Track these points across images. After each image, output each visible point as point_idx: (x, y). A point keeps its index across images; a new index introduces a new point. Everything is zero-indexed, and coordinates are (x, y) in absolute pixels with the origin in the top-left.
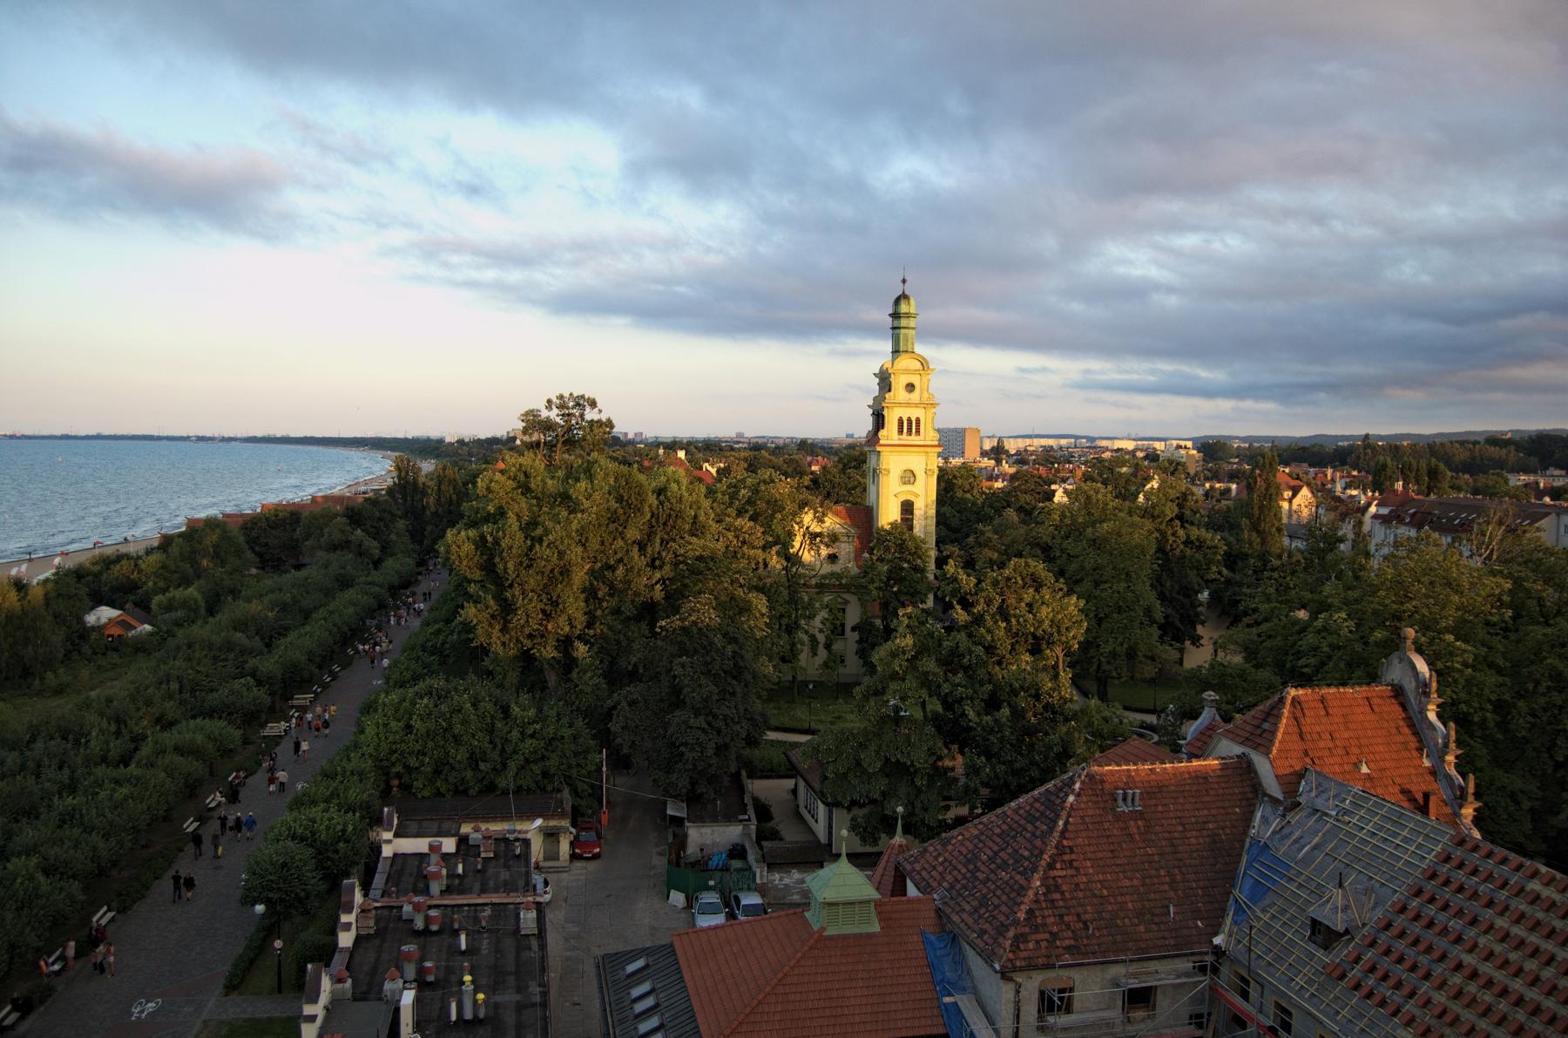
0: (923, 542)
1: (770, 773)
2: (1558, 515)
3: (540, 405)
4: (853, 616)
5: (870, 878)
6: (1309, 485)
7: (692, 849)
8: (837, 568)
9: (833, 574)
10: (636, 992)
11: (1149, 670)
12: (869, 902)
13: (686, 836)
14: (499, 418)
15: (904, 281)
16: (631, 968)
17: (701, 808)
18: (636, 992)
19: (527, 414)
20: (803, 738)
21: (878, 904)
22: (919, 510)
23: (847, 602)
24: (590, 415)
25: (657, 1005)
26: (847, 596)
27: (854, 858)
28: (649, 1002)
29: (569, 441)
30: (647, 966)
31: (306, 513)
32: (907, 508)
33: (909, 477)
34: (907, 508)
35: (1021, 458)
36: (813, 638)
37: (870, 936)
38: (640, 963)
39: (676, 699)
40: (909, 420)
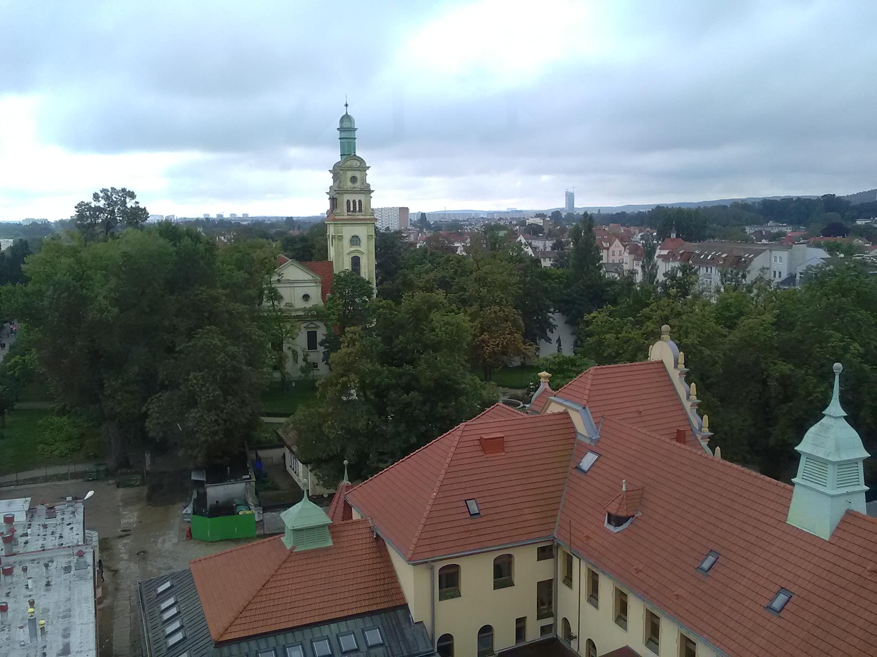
0: (368, 282)
1: (271, 446)
2: (771, 250)
3: (89, 199)
4: (321, 333)
5: (327, 513)
6: (747, 225)
7: (210, 502)
8: (309, 305)
9: (304, 309)
10: (164, 606)
11: (517, 362)
12: (323, 526)
13: (205, 493)
14: (59, 210)
15: (346, 105)
16: (160, 589)
17: (218, 475)
18: (164, 606)
19: (80, 205)
20: (282, 420)
21: (330, 527)
22: (364, 262)
23: (318, 327)
24: (130, 204)
25: (179, 613)
26: (318, 323)
27: (317, 500)
28: (174, 611)
29: (110, 220)
30: (172, 587)
31: (564, 214)
32: (356, 261)
33: (355, 240)
34: (356, 261)
35: (437, 227)
36: (295, 353)
37: (328, 548)
38: (168, 585)
39: (192, 401)
40: (354, 202)
